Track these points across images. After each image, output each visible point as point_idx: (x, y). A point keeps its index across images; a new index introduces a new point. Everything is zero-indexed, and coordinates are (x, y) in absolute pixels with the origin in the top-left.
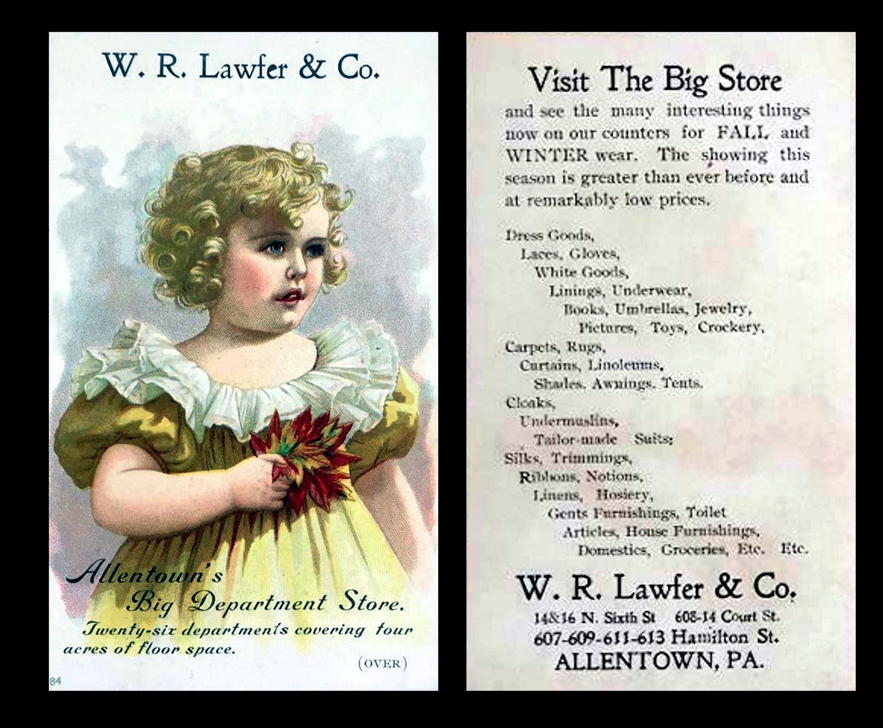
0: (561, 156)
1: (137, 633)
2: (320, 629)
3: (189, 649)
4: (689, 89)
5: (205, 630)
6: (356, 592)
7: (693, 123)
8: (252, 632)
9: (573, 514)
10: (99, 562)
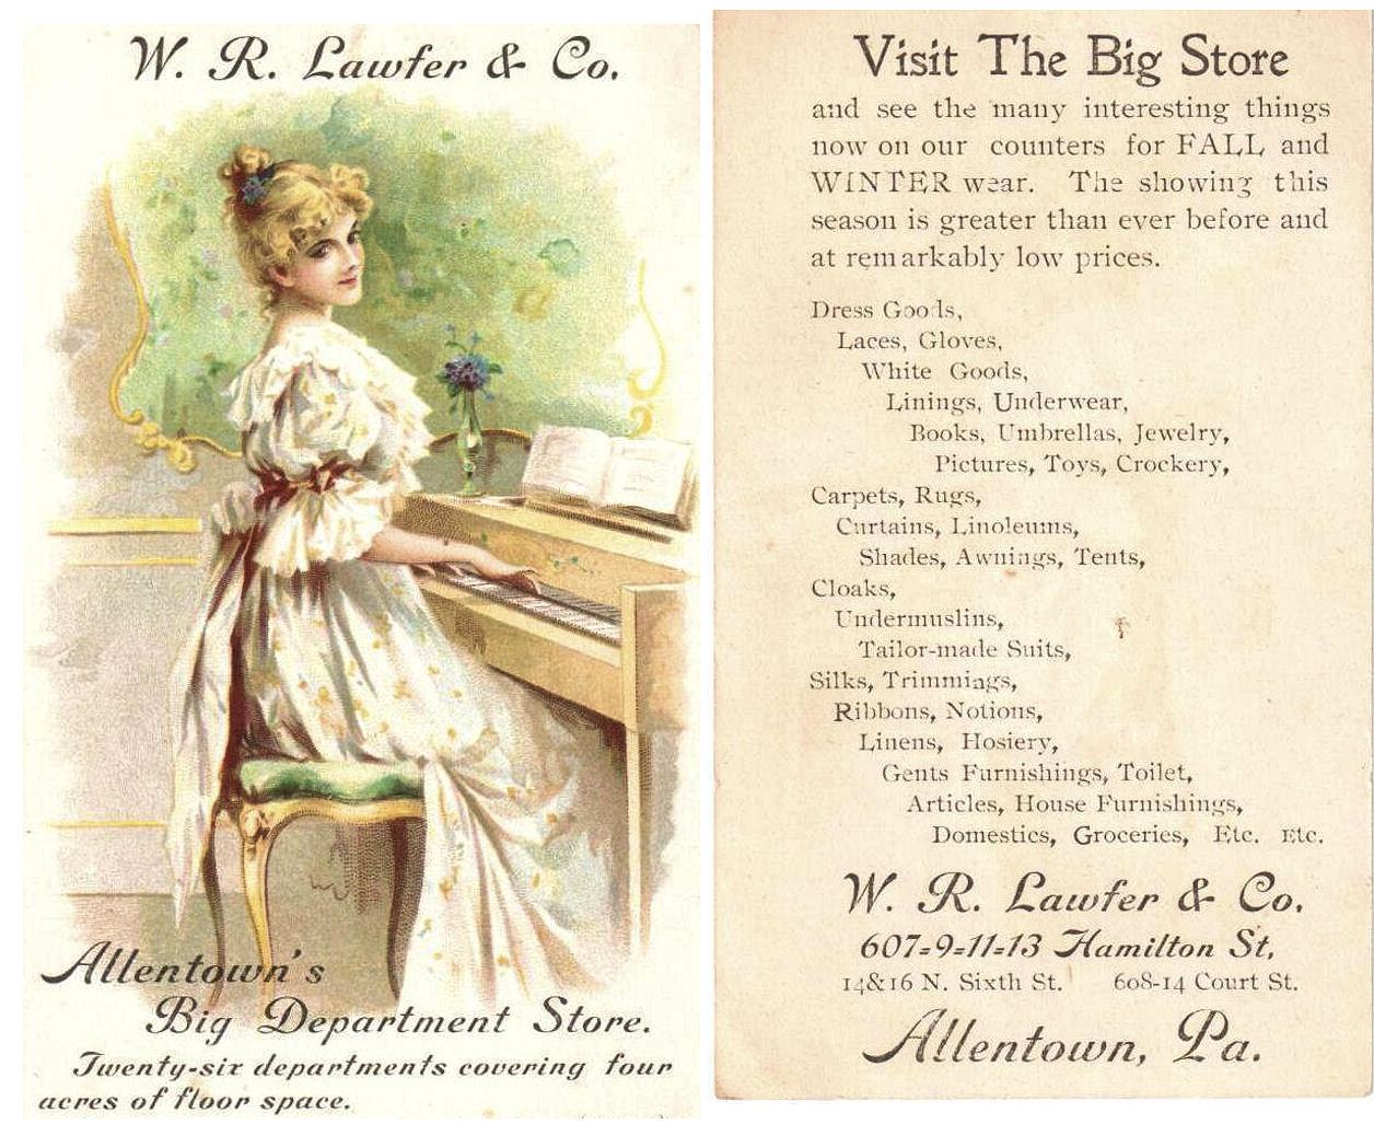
0: (904, 184)
1: (172, 1073)
2: (504, 1066)
3: (266, 1100)
4: (1129, 73)
5: (296, 1066)
6: (564, 1001)
7: (1148, 129)
8: (382, 1070)
9: (922, 775)
10: (101, 946)
